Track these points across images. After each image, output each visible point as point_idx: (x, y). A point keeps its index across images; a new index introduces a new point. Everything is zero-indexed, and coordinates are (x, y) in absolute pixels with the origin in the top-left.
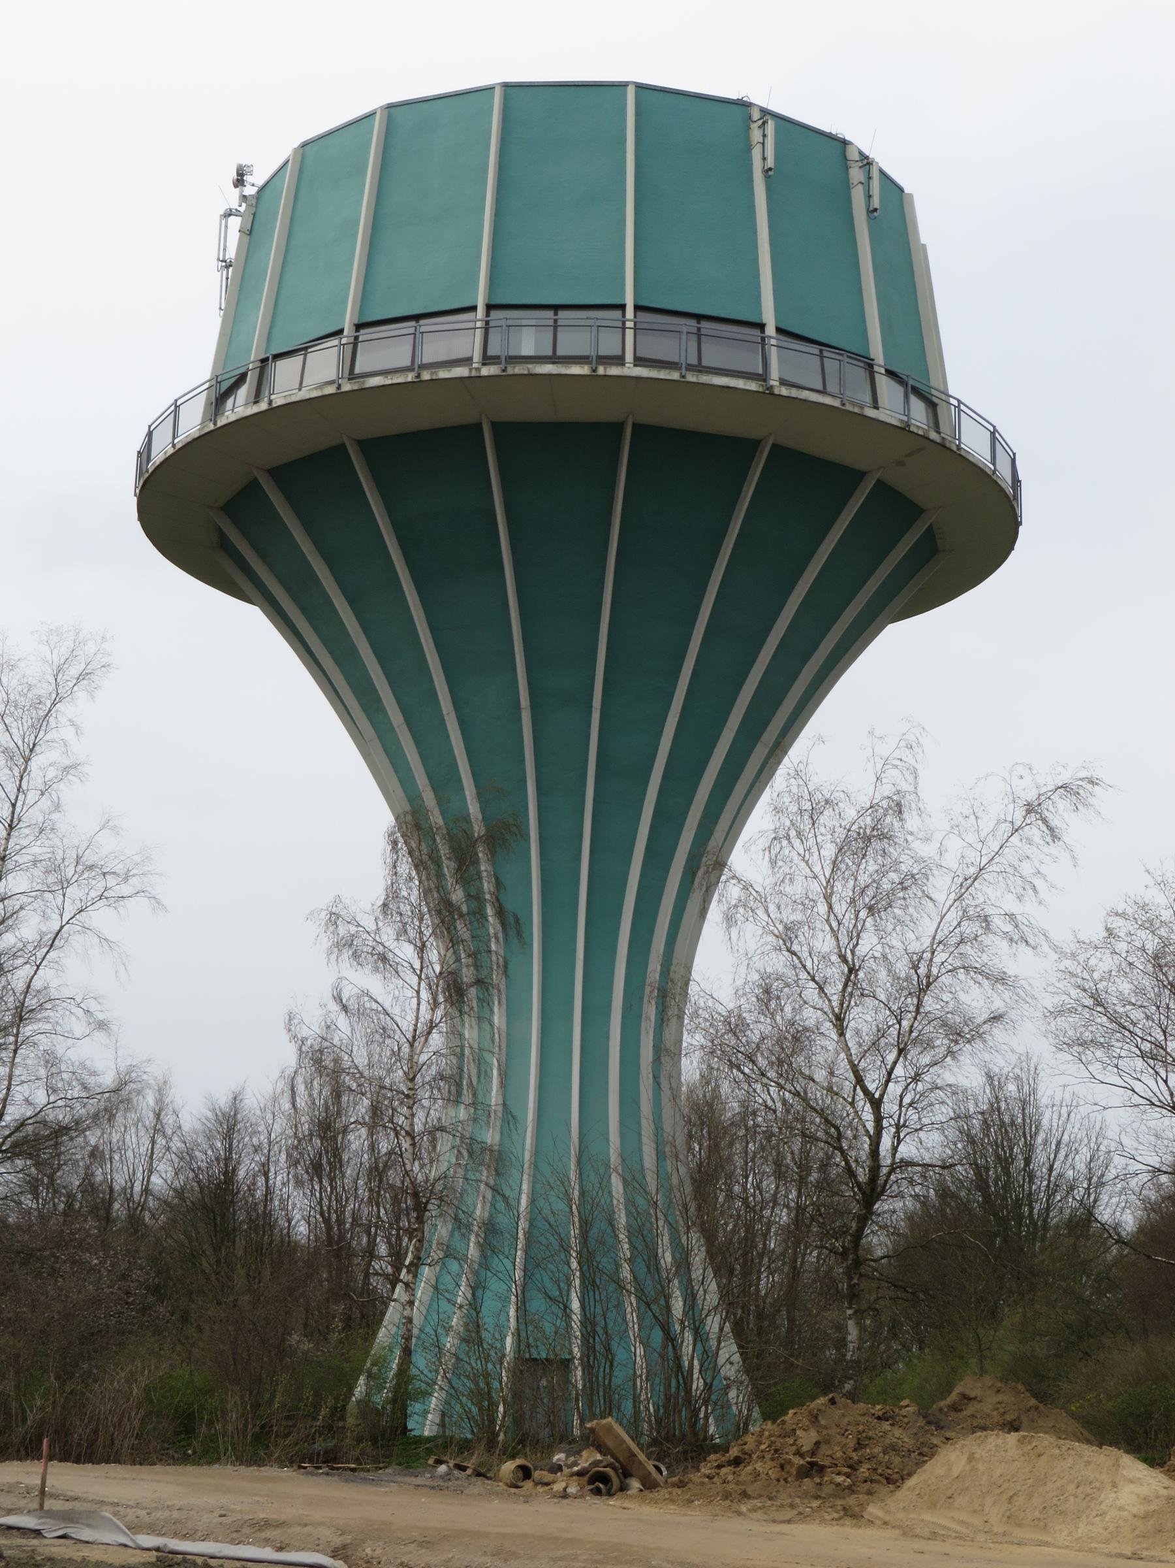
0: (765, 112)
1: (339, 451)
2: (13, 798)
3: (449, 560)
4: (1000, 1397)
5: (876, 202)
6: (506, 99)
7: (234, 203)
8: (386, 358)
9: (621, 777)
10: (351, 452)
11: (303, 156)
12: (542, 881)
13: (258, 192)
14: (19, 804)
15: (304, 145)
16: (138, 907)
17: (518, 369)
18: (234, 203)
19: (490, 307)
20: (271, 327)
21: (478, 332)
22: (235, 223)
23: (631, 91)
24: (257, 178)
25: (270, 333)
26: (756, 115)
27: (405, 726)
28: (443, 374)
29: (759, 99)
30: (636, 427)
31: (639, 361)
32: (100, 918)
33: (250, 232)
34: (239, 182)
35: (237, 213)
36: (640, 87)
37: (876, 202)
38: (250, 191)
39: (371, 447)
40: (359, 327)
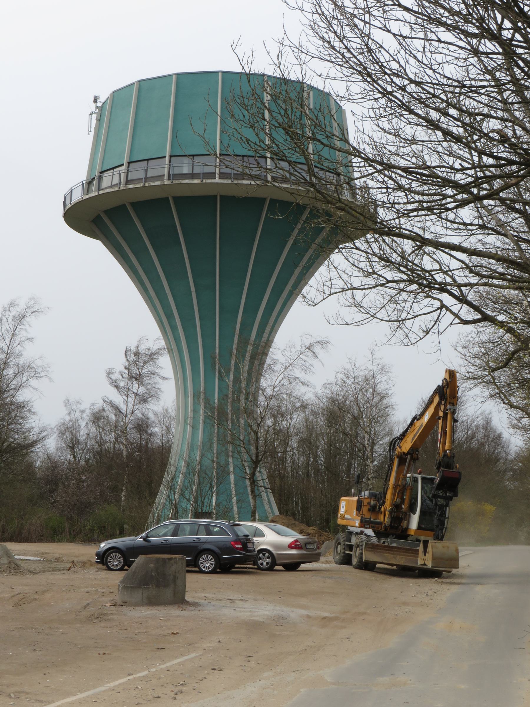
1: (167, 199)
2: (8, 345)
3: (164, 240)
4: (283, 521)
6: (177, 79)
8: (138, 173)
9: (228, 313)
10: (127, 206)
11: (113, 96)
12: (203, 350)
13: (102, 105)
14: (10, 347)
15: (114, 92)
16: (45, 379)
17: (177, 182)
19: (171, 157)
20: (103, 160)
21: (166, 168)
22: (94, 117)
23: (220, 74)
24: (102, 100)
25: (103, 162)
26: (266, 78)
27: (156, 297)
28: (152, 184)
30: (221, 196)
31: (222, 176)
32: (33, 382)
33: (100, 120)
34: (95, 101)
35: (95, 113)
36: (223, 72)
38: (99, 104)
39: (176, 199)
40: (129, 163)
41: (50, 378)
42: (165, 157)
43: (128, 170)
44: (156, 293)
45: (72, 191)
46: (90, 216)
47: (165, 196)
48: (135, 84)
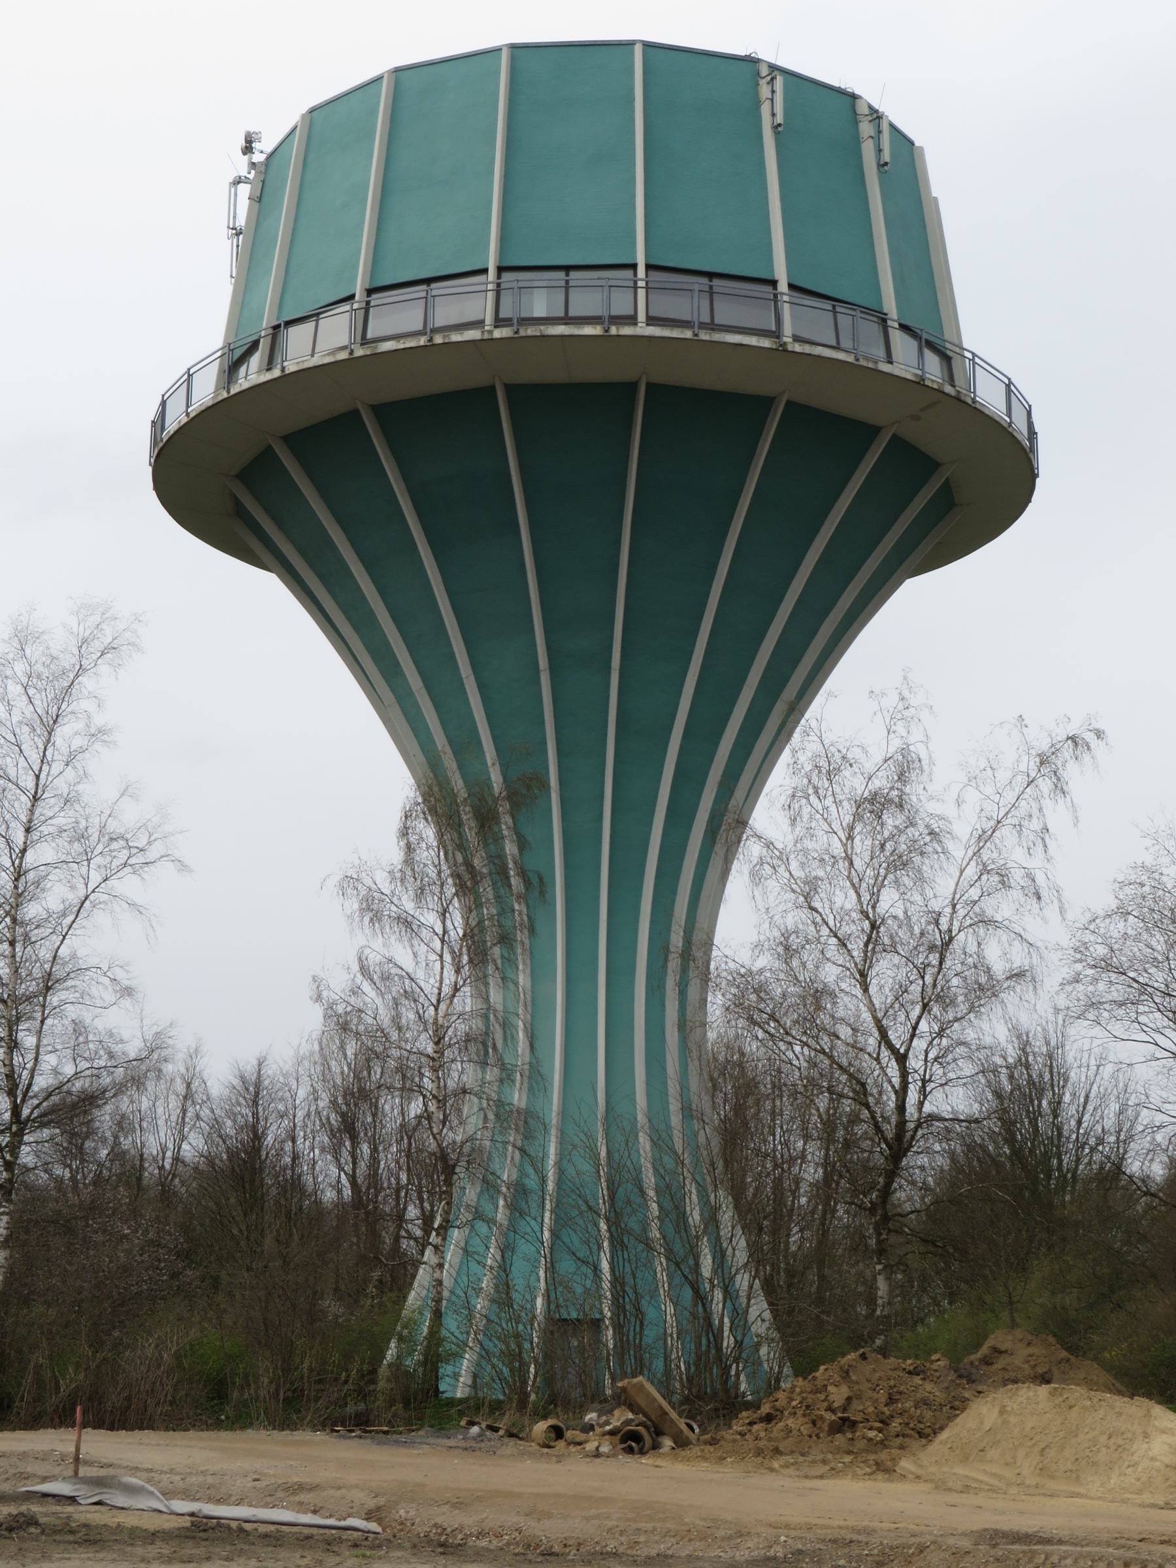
0: (773, 68)
2: (36, 768)
3: (466, 524)
5: (886, 156)
6: (513, 60)
7: (243, 171)
8: (398, 322)
9: (642, 736)
13: (267, 159)
15: (312, 111)
16: (165, 869)
17: (531, 331)
18: (243, 171)
19: (501, 270)
20: (283, 294)
22: (244, 190)
23: (638, 50)
24: (266, 145)
26: (764, 71)
27: (424, 691)
29: (767, 54)
31: (651, 320)
32: (125, 885)
34: (248, 149)
35: (246, 181)
36: (647, 45)
37: (886, 156)
38: (258, 158)
40: (370, 292)
41: (182, 866)
42: (485, 271)
43: (368, 303)
44: (424, 681)
45: (190, 376)
46: (240, 473)
47: (482, 380)
48: (385, 80)
